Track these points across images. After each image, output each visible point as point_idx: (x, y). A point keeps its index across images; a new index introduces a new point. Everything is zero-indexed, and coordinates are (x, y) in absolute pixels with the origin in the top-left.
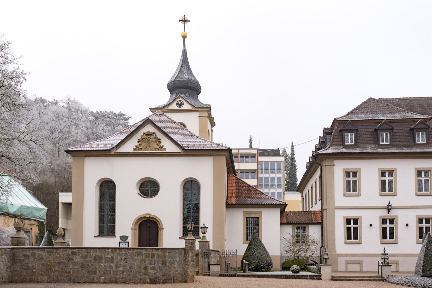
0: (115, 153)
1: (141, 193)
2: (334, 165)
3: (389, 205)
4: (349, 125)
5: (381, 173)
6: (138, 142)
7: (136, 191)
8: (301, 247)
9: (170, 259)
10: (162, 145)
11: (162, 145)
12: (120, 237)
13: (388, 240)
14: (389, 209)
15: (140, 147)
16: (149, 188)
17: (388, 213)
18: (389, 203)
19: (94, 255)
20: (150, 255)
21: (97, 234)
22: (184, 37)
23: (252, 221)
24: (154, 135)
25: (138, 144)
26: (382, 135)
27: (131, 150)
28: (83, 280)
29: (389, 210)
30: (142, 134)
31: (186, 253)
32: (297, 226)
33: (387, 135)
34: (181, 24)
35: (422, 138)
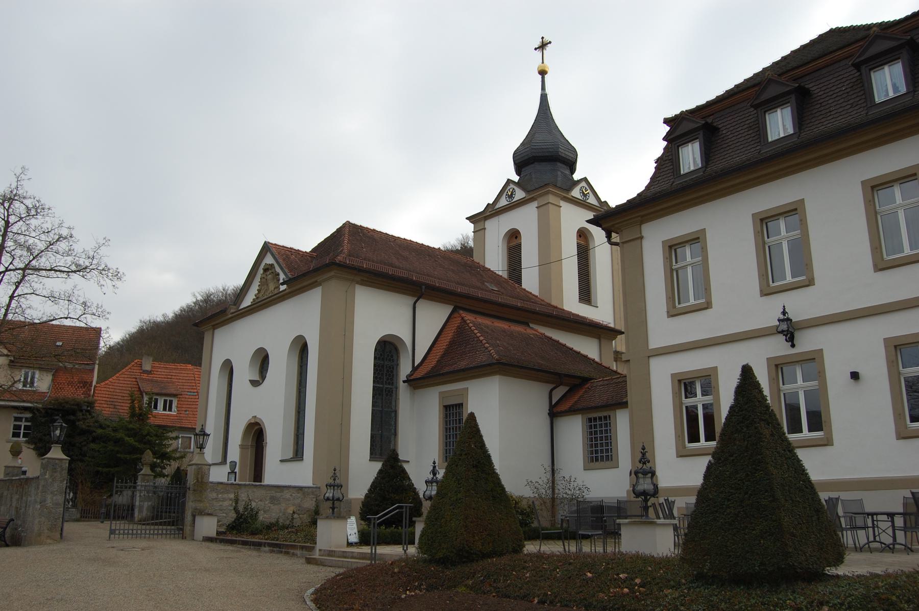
3: (785, 319)
8: (41, 488)
14: (789, 330)
17: (793, 346)
18: (784, 313)
21: (290, 455)
22: (543, 73)
28: (287, 494)
29: (791, 339)
34: (538, 53)
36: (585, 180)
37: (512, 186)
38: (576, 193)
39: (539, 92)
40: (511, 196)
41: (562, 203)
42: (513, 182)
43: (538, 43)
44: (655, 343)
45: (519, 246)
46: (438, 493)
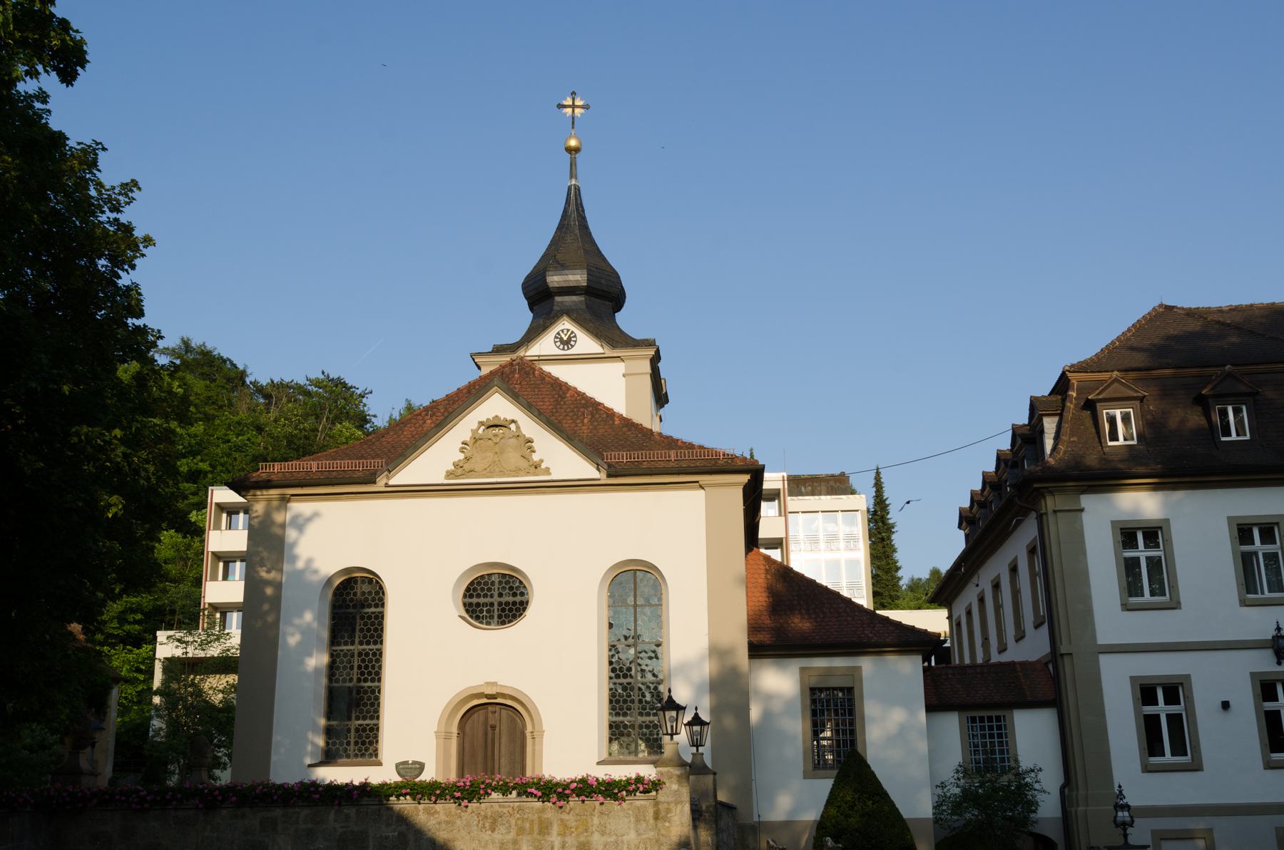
0: (387, 485)
1: (467, 611)
2: (1082, 510)
4: (1116, 384)
5: (1120, 538)
6: (462, 450)
7: (452, 608)
9: (605, 839)
10: (536, 457)
11: (536, 457)
12: (397, 765)
13: (1168, 757)
15: (467, 467)
16: (495, 598)
19: (340, 830)
20: (536, 827)
23: (828, 701)
24: (513, 426)
25: (462, 456)
26: (1224, 414)
27: (439, 478)
30: (475, 426)
31: (663, 813)
32: (977, 714)
33: (1237, 412)
35: (1240, 423)
40: (567, 343)
44: (1102, 639)
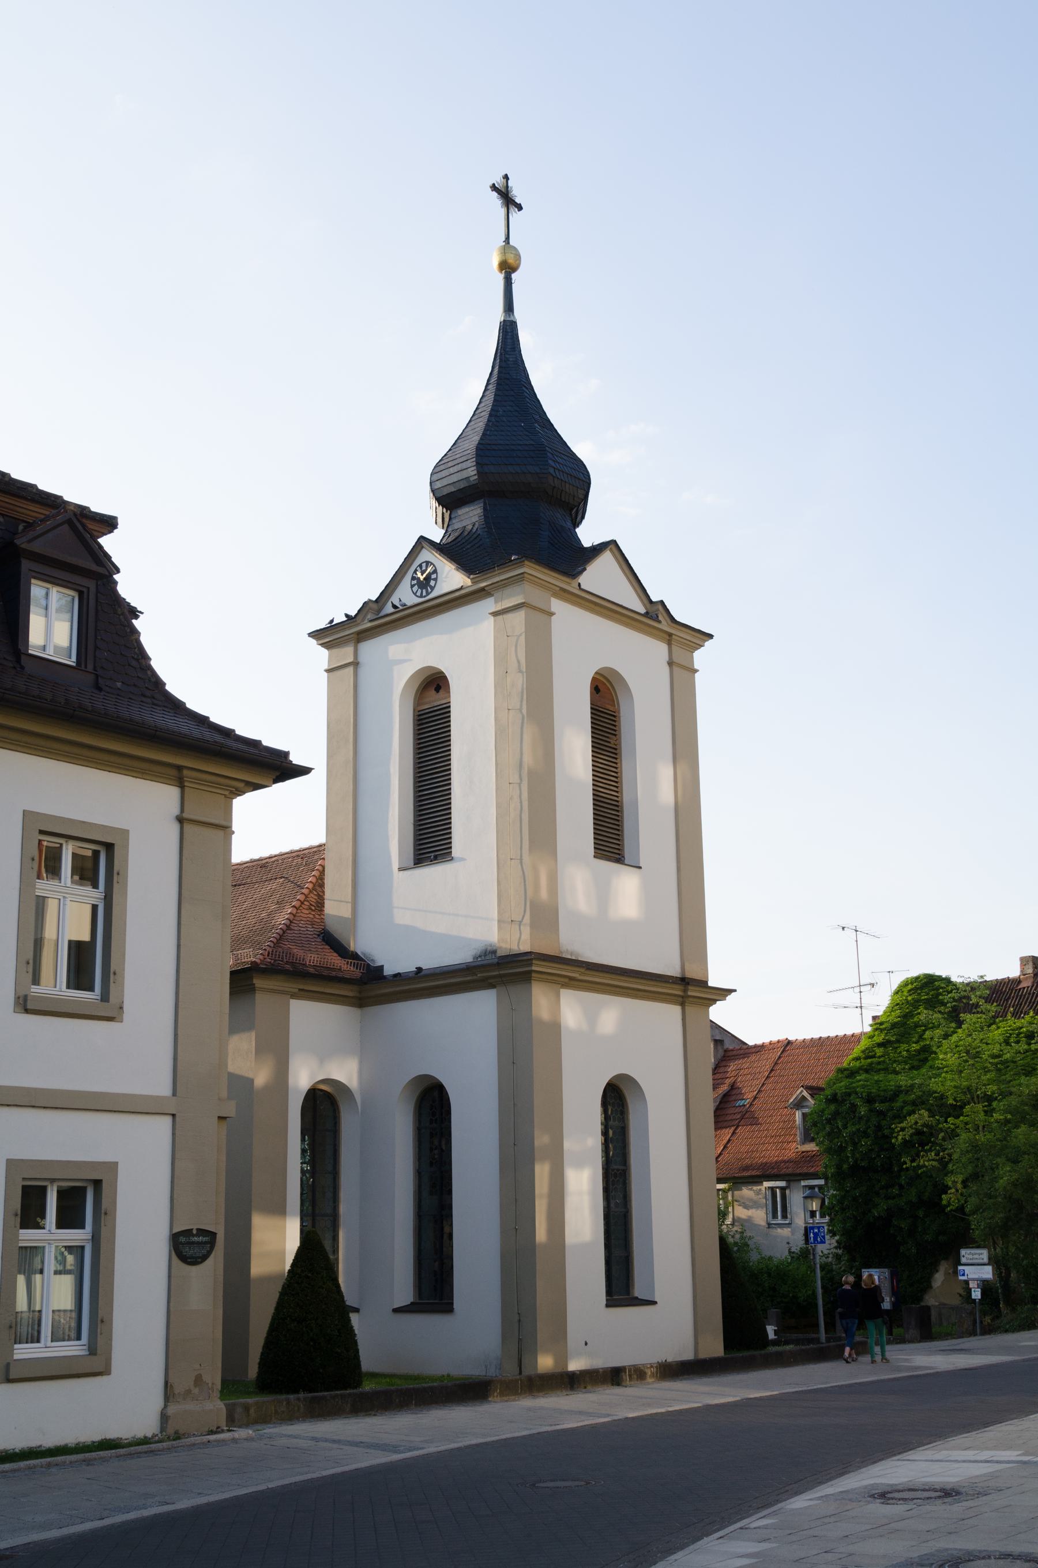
36: (612, 545)
37: (427, 555)
38: (599, 577)
39: (498, 315)
40: (425, 584)
41: (557, 605)
42: (431, 543)
43: (518, 194)
45: (443, 714)
46: (982, 1294)
